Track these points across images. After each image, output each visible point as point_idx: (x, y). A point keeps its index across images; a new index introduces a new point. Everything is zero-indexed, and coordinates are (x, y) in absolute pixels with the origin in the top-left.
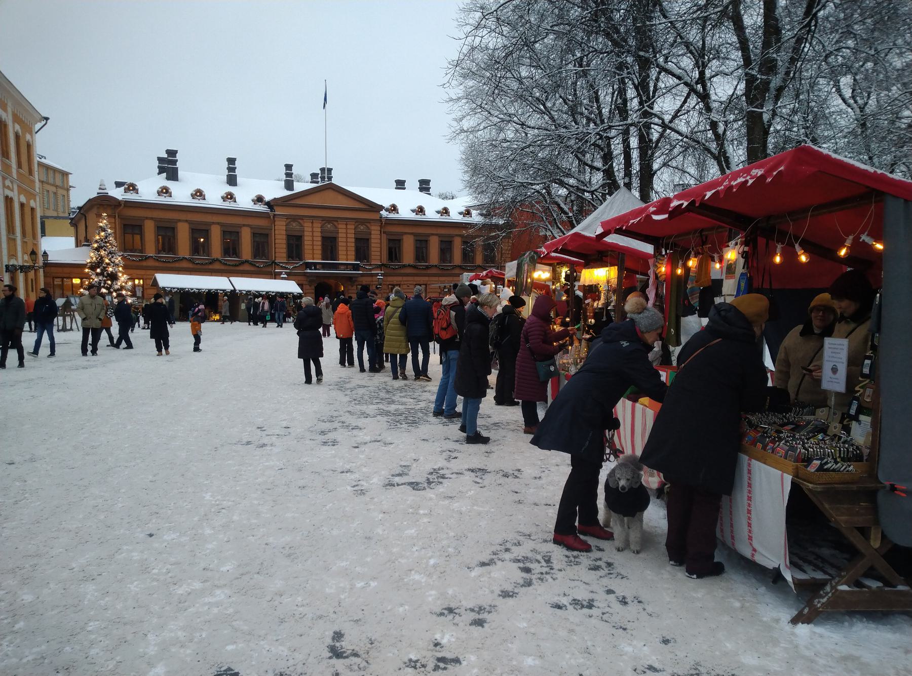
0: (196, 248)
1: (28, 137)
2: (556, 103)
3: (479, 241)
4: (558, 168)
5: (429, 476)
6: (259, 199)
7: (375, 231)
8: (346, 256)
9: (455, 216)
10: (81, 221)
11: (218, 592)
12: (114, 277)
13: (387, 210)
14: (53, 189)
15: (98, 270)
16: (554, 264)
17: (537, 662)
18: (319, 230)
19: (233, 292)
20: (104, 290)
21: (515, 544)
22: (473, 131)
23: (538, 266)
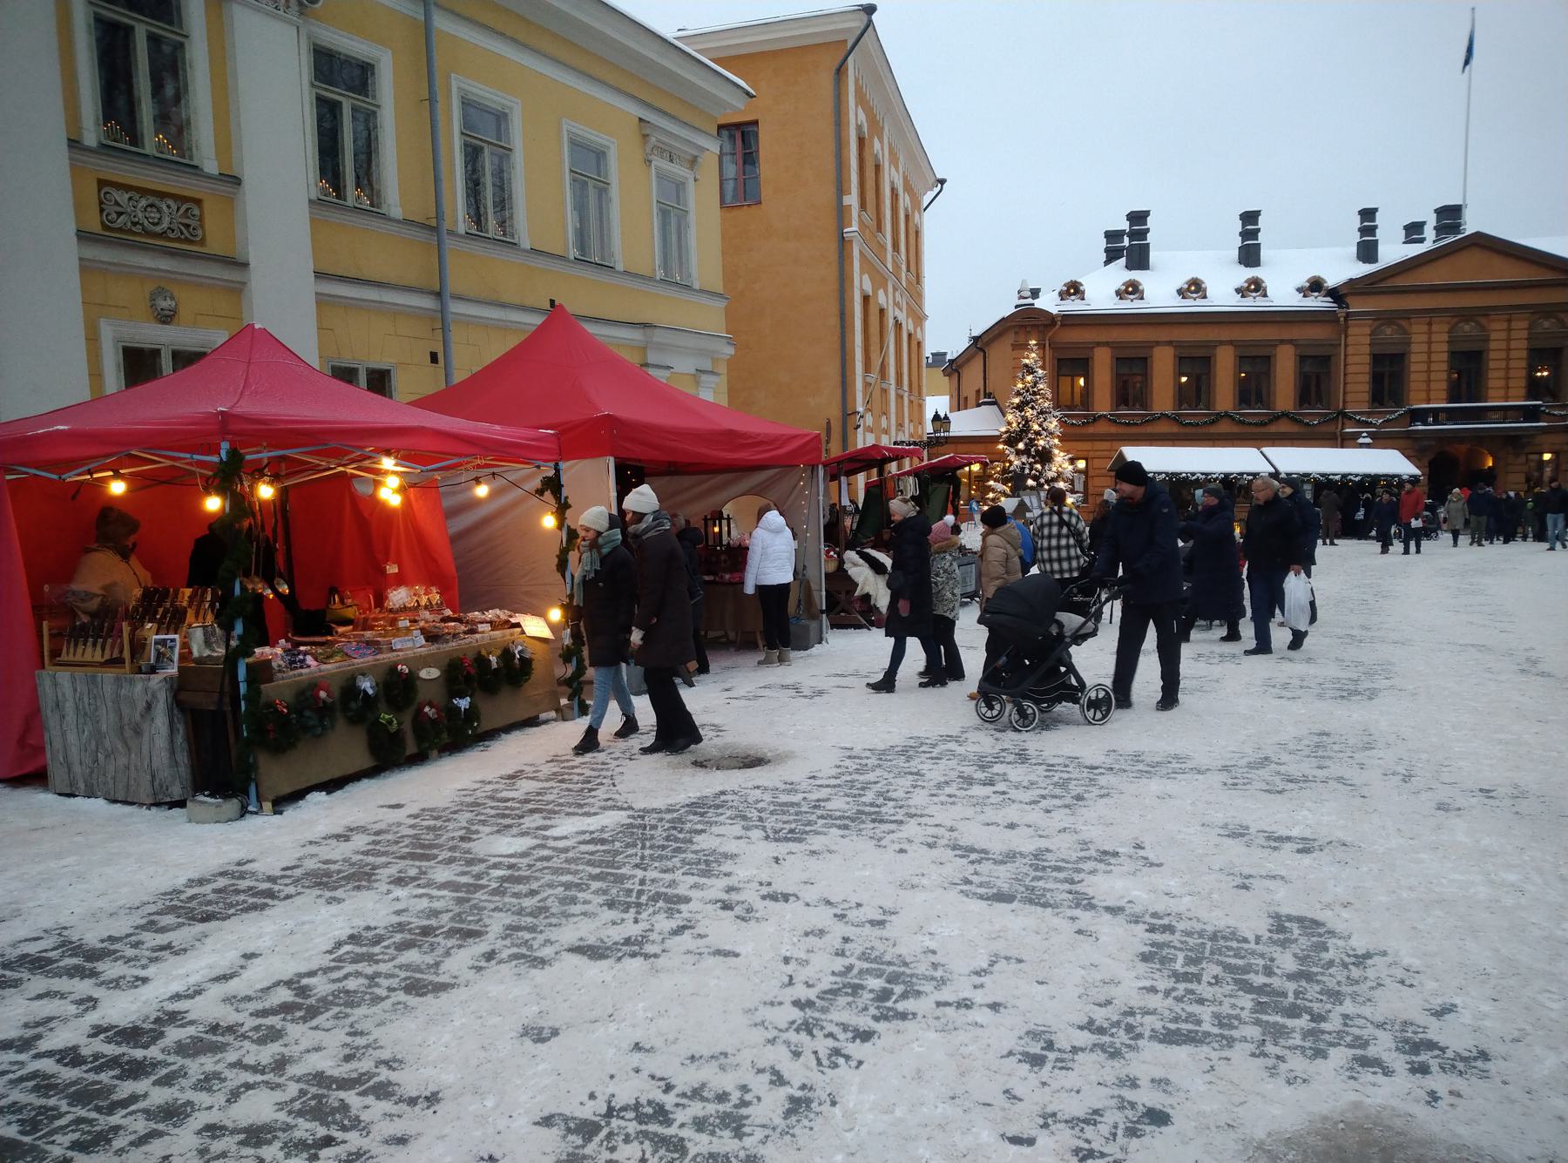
6: (1316, 285)
12: (1045, 457)
15: (1021, 446)
18: (1445, 337)
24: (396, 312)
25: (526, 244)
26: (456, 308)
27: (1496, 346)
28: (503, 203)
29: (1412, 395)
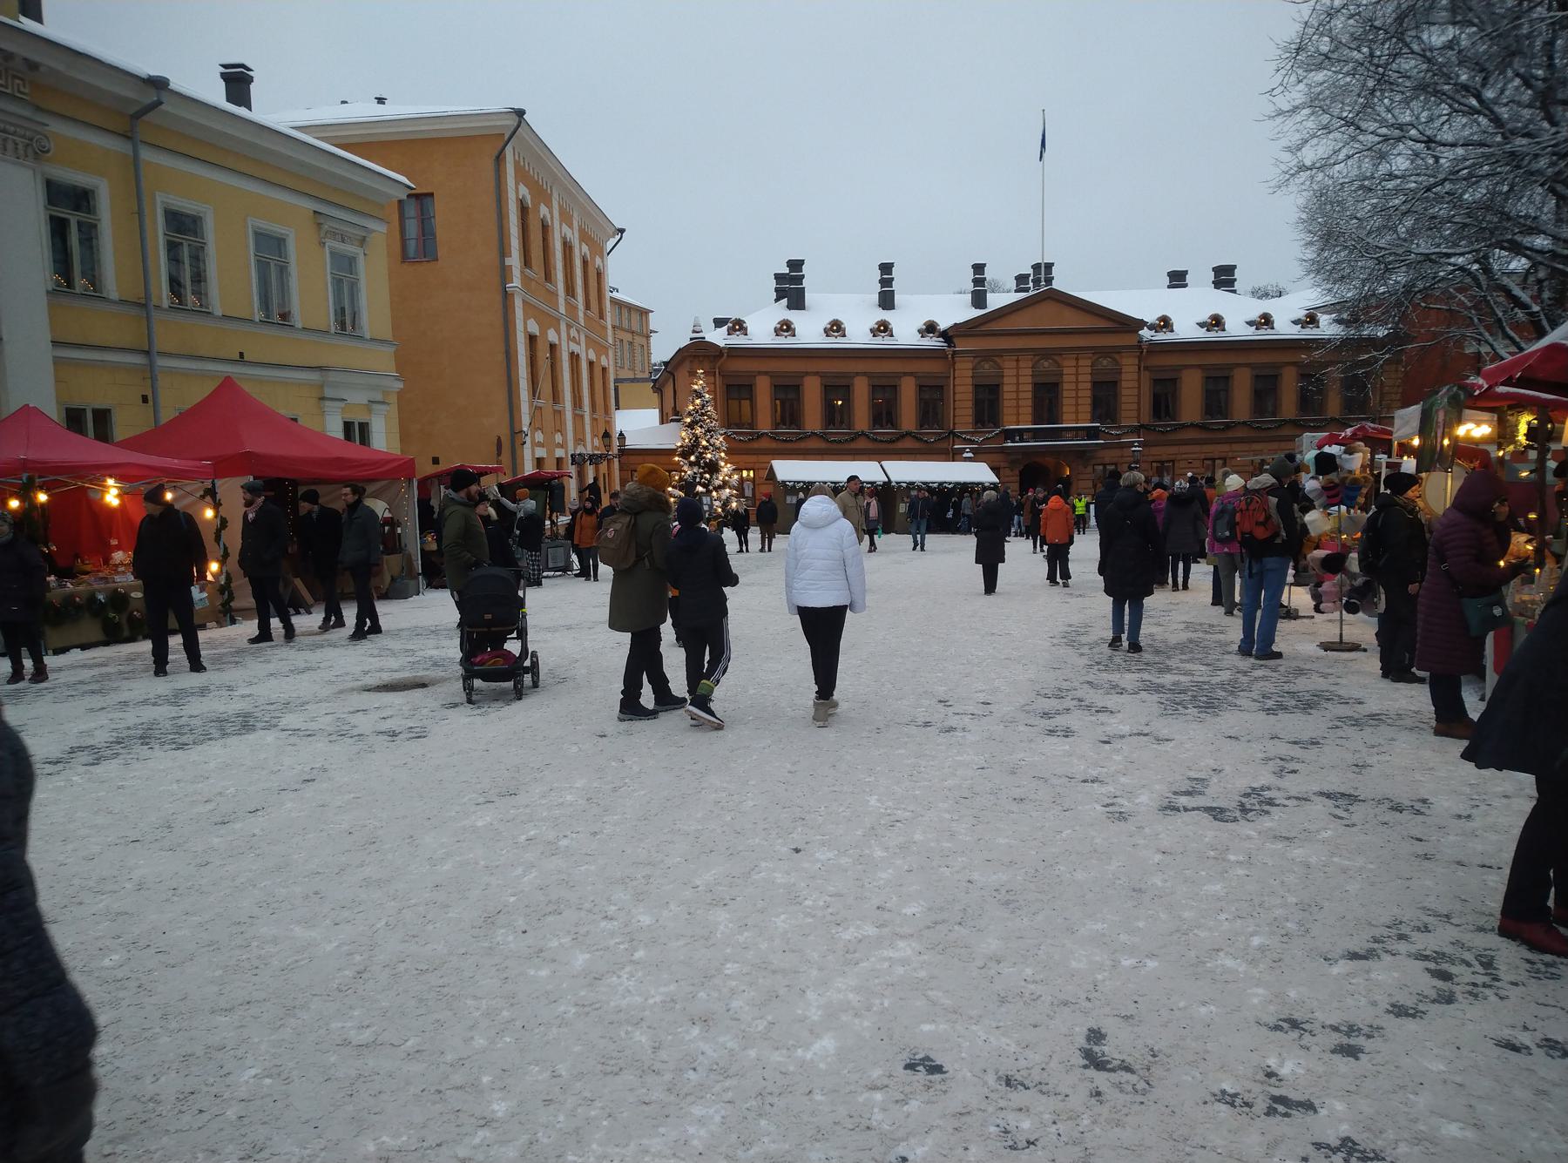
0: (833, 416)
1: (598, 261)
2: (1507, 92)
3: (1335, 372)
4: (1509, 219)
5: (1244, 800)
6: (930, 328)
7: (1129, 365)
8: (1076, 415)
9: (1284, 328)
10: (667, 384)
11: (901, 944)
12: (713, 468)
13: (1152, 327)
14: (628, 337)
15: (692, 458)
16: (1502, 410)
17: (1470, 1134)
19: (887, 484)
20: (700, 489)
21: (1419, 929)
22: (1323, 165)
23: (1467, 412)
24: (116, 367)
25: (218, 312)
26: (161, 362)
27: (1008, 389)
28: (199, 278)
29: (1006, 418)
